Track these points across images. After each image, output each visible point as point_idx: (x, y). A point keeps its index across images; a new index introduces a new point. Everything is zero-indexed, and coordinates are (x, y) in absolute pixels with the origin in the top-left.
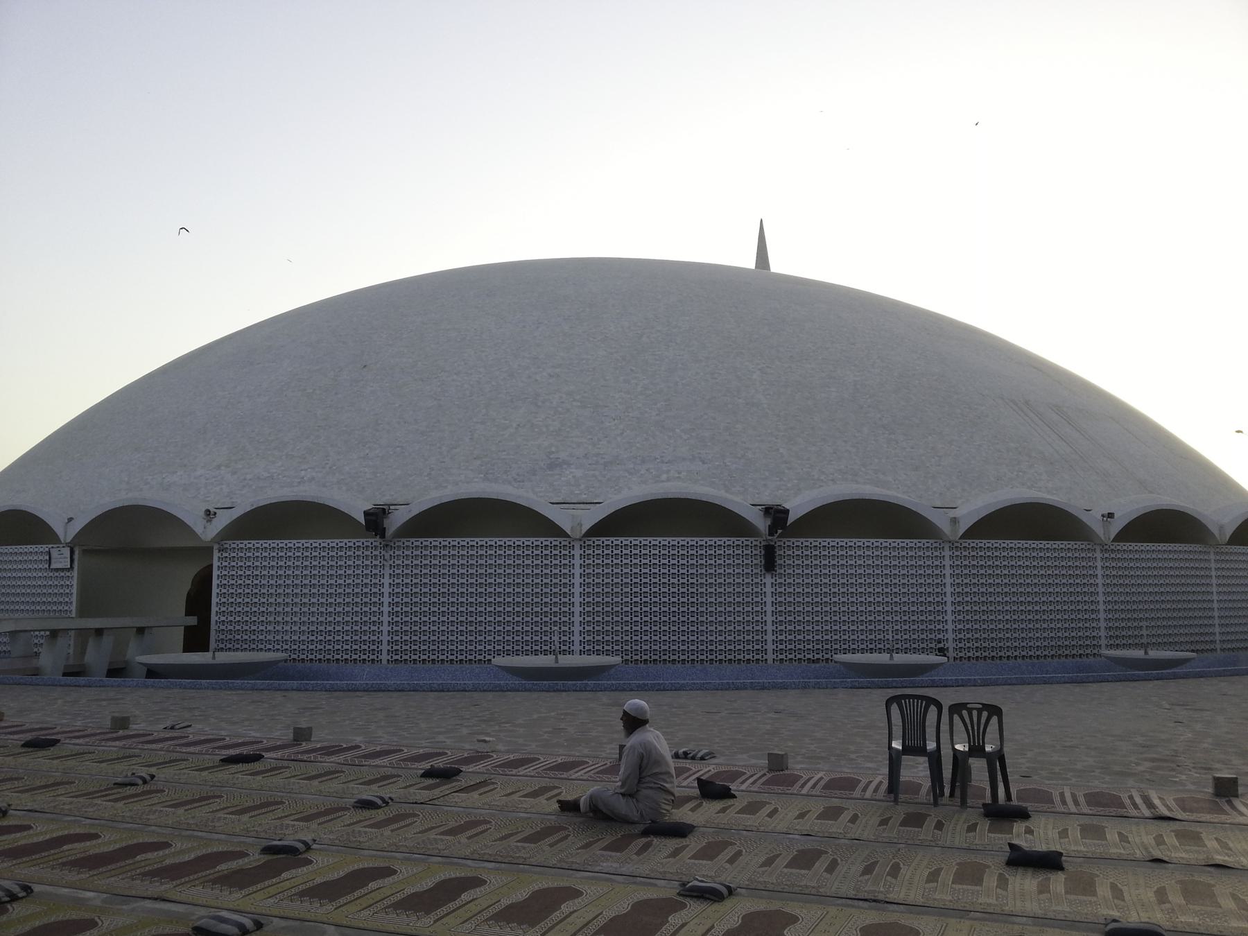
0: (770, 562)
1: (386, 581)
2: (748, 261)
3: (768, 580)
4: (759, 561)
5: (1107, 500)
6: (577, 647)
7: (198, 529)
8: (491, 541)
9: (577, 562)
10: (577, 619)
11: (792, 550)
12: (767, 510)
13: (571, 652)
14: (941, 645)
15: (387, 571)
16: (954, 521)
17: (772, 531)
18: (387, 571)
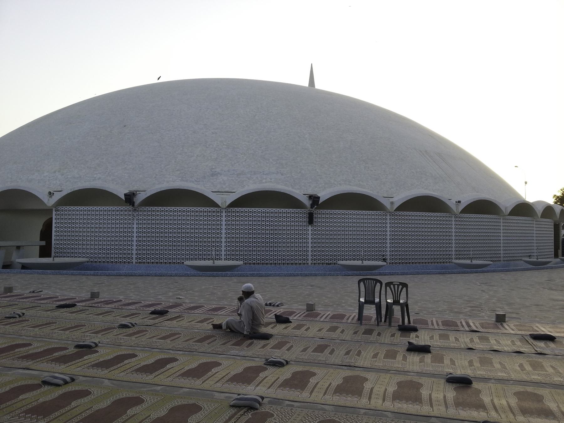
0: (311, 221)
1: (135, 226)
2: (306, 83)
3: (310, 228)
4: (306, 219)
5: (457, 195)
6: (223, 257)
7: (45, 201)
8: (102, 208)
9: (224, 219)
10: (223, 244)
11: (321, 215)
12: (310, 197)
13: (221, 259)
14: (384, 257)
15: (135, 222)
16: (392, 203)
17: (312, 206)
18: (135, 222)
